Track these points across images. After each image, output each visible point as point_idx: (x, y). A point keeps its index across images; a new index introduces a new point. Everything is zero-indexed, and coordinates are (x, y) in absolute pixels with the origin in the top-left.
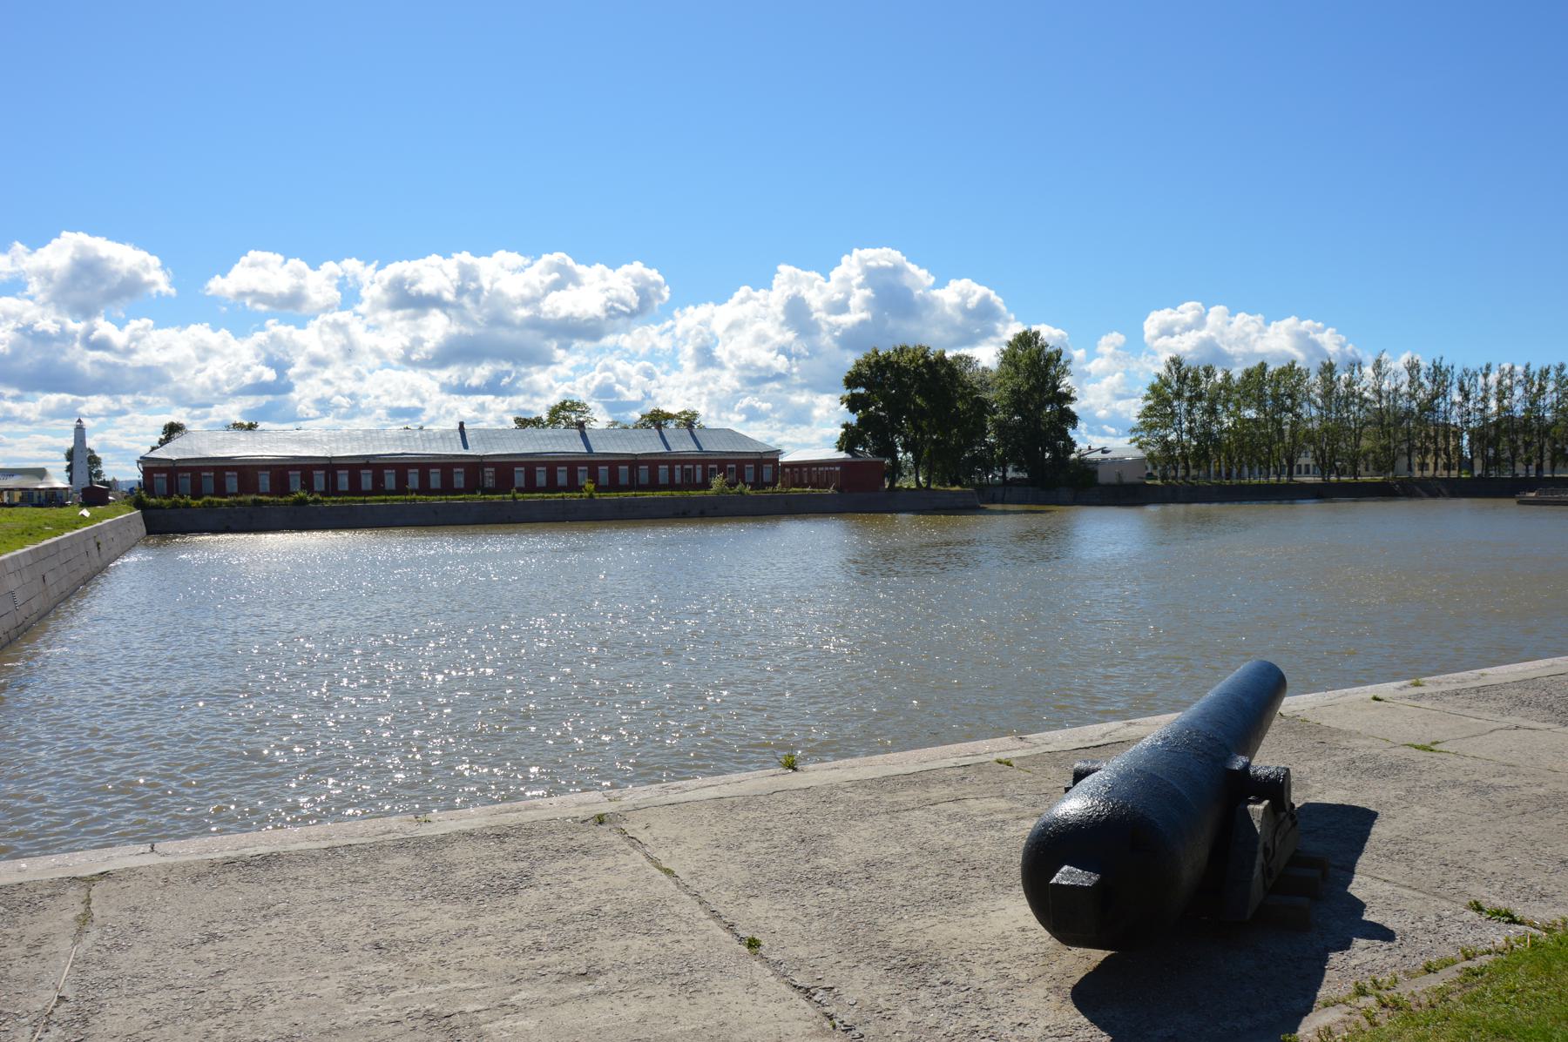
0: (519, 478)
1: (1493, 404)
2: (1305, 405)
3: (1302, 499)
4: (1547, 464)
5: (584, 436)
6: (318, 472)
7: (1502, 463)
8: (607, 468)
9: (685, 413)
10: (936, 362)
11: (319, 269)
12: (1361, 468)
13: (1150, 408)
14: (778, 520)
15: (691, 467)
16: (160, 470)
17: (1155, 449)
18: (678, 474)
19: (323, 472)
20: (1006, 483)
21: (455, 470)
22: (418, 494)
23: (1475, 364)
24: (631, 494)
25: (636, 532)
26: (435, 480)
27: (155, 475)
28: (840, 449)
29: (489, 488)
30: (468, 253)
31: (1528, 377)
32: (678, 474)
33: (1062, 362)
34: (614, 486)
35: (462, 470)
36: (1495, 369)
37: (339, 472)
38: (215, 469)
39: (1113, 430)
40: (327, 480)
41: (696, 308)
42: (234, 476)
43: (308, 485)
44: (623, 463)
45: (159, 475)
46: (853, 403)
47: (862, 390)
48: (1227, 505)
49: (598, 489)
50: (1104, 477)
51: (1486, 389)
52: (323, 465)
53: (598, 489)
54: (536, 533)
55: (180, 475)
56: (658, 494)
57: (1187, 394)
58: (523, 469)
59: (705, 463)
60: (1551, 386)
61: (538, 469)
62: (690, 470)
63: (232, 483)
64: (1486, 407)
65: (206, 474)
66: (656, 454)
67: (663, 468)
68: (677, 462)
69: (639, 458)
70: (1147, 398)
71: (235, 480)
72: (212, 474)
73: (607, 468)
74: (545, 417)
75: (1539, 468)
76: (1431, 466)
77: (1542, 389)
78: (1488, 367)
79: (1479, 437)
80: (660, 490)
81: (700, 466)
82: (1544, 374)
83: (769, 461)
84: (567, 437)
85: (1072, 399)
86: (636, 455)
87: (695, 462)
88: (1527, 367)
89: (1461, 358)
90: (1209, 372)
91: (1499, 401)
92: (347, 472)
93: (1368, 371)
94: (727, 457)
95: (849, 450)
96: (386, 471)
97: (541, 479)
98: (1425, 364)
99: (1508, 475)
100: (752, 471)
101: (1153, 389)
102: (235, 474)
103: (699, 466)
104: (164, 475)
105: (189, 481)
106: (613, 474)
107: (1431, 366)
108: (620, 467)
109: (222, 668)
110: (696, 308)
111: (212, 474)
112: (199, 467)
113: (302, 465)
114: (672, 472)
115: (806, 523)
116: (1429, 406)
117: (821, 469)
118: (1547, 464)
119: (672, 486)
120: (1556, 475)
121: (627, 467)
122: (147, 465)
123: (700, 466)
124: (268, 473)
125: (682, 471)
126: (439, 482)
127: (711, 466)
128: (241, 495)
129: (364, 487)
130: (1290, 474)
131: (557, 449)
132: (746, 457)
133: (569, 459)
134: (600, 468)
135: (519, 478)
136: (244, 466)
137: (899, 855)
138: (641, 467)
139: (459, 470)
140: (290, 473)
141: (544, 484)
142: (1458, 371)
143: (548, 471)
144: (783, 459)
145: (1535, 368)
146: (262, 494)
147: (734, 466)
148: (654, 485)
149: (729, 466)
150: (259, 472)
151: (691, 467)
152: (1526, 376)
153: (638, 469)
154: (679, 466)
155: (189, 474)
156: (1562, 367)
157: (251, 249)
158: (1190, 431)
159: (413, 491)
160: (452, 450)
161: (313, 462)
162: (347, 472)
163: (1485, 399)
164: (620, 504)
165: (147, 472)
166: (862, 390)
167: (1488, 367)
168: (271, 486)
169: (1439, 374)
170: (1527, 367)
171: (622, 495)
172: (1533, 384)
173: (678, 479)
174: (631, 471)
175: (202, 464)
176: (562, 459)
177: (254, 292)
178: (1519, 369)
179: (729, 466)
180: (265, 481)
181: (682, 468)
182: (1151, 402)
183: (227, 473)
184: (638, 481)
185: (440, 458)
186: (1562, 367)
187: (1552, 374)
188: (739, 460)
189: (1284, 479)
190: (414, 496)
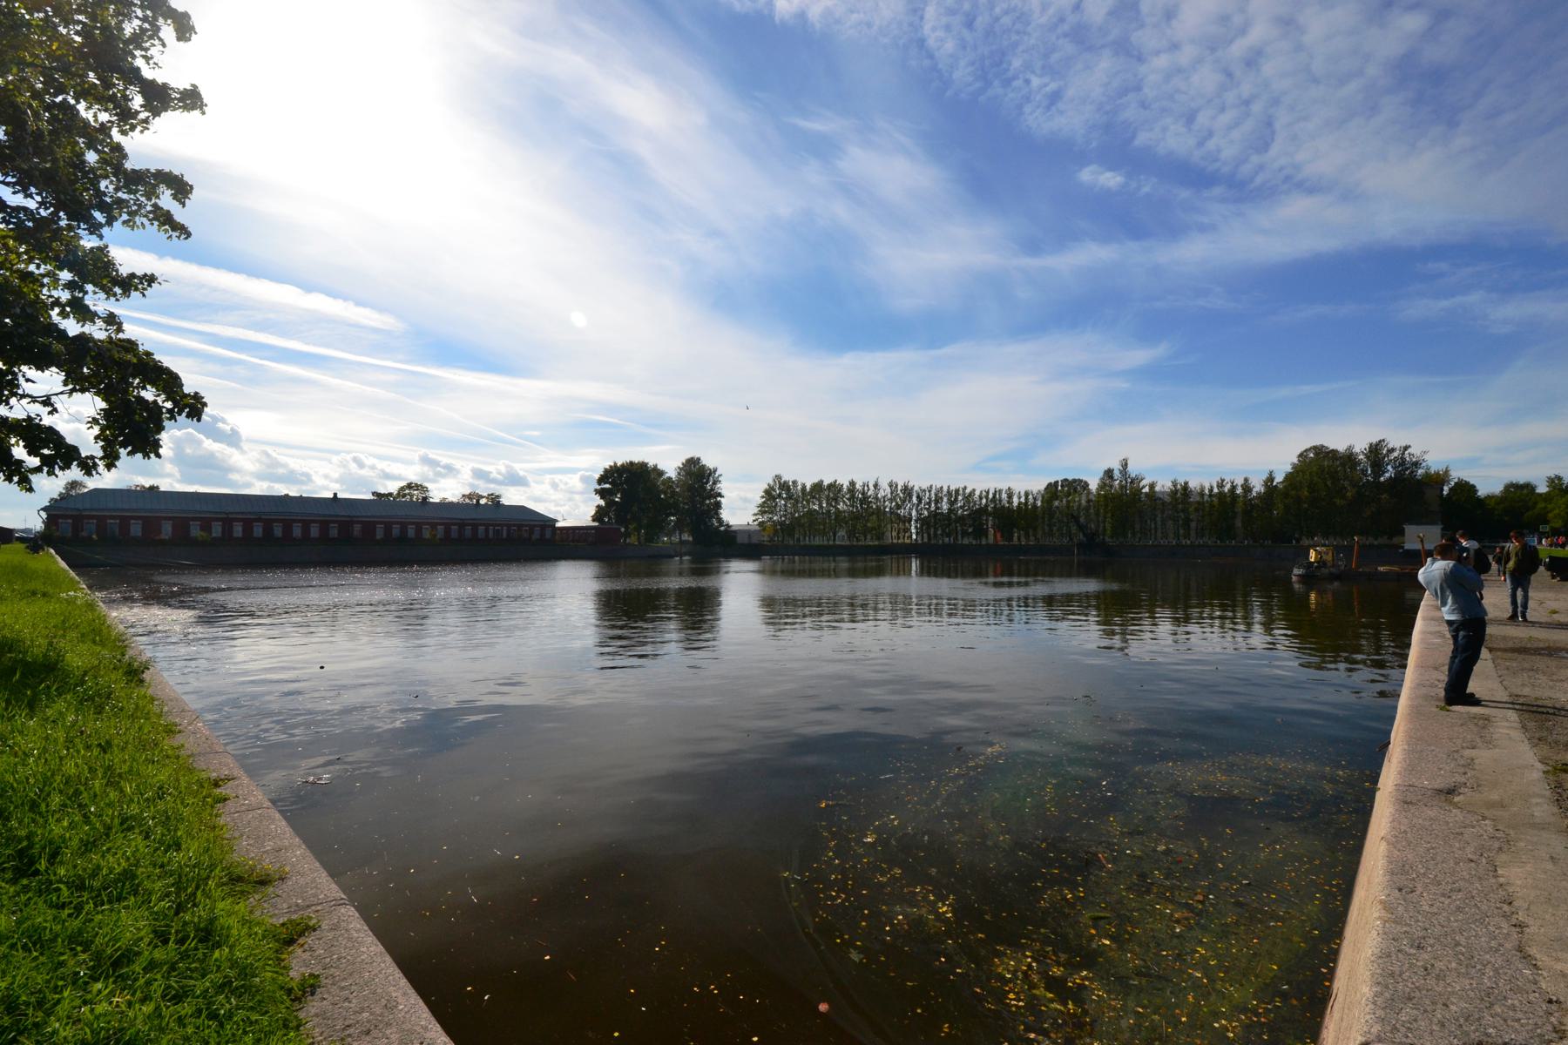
2: (841, 504)
7: (9, 723)
9: (492, 495)
13: (764, 502)
15: (499, 528)
25: (361, 573)
28: (594, 520)
31: (949, 493)
33: (717, 475)
37: (235, 523)
41: (699, 459)
46: (602, 493)
47: (607, 486)
50: (740, 540)
55: (86, 521)
60: (960, 498)
64: (930, 507)
67: (482, 529)
68: (492, 525)
70: (763, 497)
77: (956, 499)
78: (931, 487)
82: (957, 491)
83: (549, 526)
88: (721, 475)
91: (936, 504)
93: (872, 488)
99: (984, 542)
101: (767, 492)
104: (70, 521)
110: (699, 459)
111: (118, 521)
114: (487, 531)
117: (582, 531)
124: (171, 522)
130: (834, 540)
132: (376, 520)
142: (916, 488)
144: (558, 525)
151: (499, 528)
163: (929, 503)
166: (607, 486)
167: (931, 487)
169: (907, 491)
170: (949, 487)
178: (945, 489)
183: (132, 521)
189: (831, 543)
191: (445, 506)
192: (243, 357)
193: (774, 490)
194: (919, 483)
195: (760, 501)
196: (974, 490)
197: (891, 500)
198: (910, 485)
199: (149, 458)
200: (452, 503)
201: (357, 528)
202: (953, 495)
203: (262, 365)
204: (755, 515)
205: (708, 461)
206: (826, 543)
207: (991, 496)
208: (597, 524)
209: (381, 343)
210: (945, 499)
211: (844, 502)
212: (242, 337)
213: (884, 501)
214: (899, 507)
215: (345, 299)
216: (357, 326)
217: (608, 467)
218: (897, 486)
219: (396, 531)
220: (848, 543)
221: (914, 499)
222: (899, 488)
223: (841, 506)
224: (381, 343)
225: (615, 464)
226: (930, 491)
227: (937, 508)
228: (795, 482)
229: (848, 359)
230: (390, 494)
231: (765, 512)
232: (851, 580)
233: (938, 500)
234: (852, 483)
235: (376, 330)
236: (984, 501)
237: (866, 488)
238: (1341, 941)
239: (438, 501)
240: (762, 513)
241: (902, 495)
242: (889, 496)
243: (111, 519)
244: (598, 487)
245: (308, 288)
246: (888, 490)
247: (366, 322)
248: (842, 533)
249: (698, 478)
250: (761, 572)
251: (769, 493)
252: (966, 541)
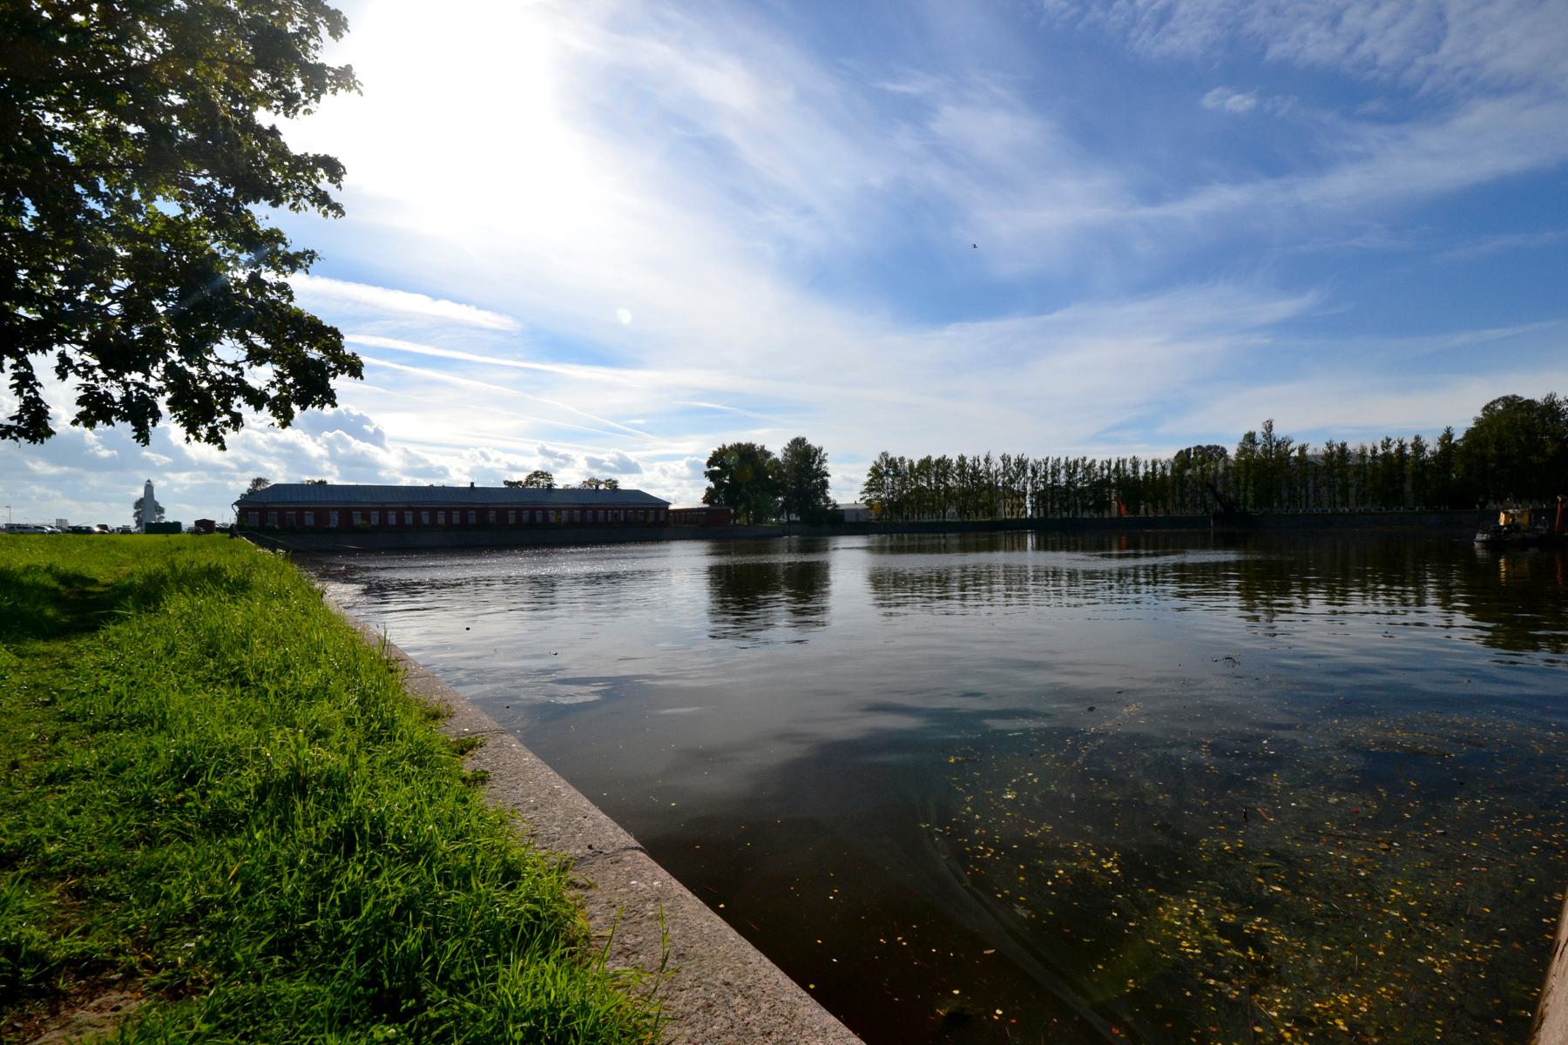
1: (1197, 951)
4: (1079, 510)
12: (980, 513)
18: (610, 515)
20: (790, 522)
28: (704, 502)
31: (1067, 465)
41: (804, 439)
47: (717, 468)
51: (1046, 472)
57: (892, 473)
60: (1079, 470)
67: (601, 513)
70: (870, 475)
75: (1076, 512)
77: (1075, 471)
78: (1047, 459)
79: (1040, 497)
82: (1076, 462)
85: (706, 473)
93: (982, 462)
104: (257, 513)
114: (606, 514)
118: (1079, 510)
130: (944, 517)
137: (770, 1008)
142: (1031, 462)
144: (671, 507)
145: (1071, 459)
160: (343, 476)
163: (1045, 477)
166: (717, 468)
167: (1047, 459)
169: (1021, 464)
178: (1063, 461)
185: (941, 580)
186: (1269, 426)
189: (941, 520)
191: (568, 492)
192: (385, 363)
193: (881, 468)
194: (1034, 455)
195: (867, 479)
196: (1094, 461)
197: (1004, 474)
198: (1025, 458)
199: (1003, 459)
200: (573, 490)
202: (1071, 468)
203: (401, 370)
204: (863, 493)
205: (813, 441)
207: (1113, 467)
208: (707, 506)
209: (502, 344)
210: (1063, 472)
211: (954, 478)
212: (383, 345)
213: (996, 476)
214: (1012, 481)
215: (468, 304)
216: (481, 329)
217: (716, 450)
218: (1009, 460)
219: (526, 516)
220: (958, 520)
221: (1029, 474)
222: (1013, 461)
223: (951, 482)
224: (502, 344)
225: (724, 446)
226: (1046, 464)
227: (1054, 481)
228: (902, 459)
229: (952, 331)
230: (520, 483)
231: (872, 490)
233: (1055, 472)
234: (962, 458)
235: (495, 332)
236: (1106, 472)
237: (977, 463)
239: (561, 487)
240: (869, 491)
241: (1015, 469)
242: (1002, 470)
244: (708, 470)
245: (436, 296)
246: (1001, 464)
247: (487, 324)
248: (952, 510)
249: (804, 458)
250: (869, 549)
251: (875, 471)
252: (1086, 515)
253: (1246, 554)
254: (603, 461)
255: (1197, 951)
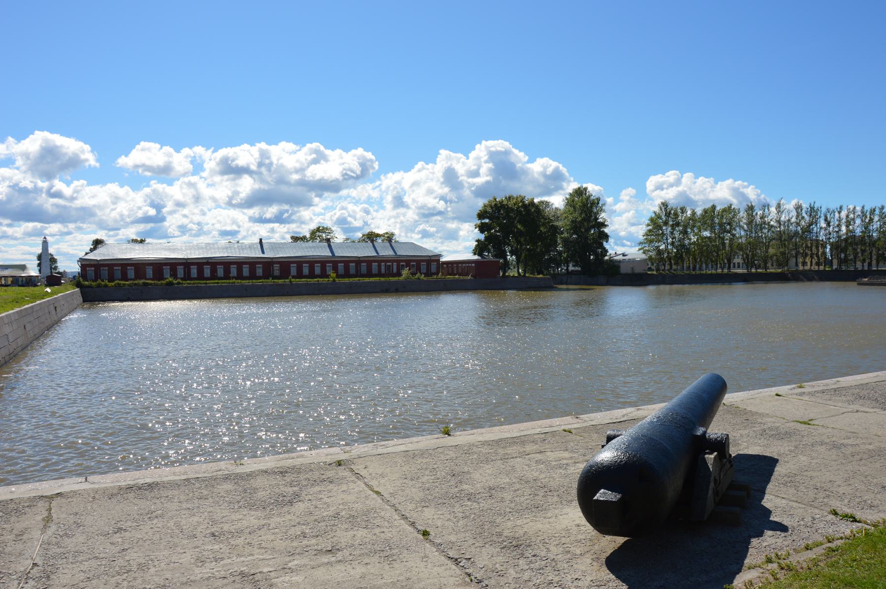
0: (293, 270)
1: (844, 229)
3: (736, 282)
4: (874, 262)
5: (330, 246)
6: (180, 267)
8: (343, 264)
10: (529, 205)
11: (180, 152)
14: (439, 294)
15: (391, 264)
16: (90, 266)
17: (653, 254)
18: (383, 268)
19: (182, 267)
20: (568, 273)
21: (257, 266)
22: (236, 279)
23: (834, 206)
24: (357, 279)
25: (359, 301)
26: (246, 271)
27: (88, 269)
28: (475, 254)
29: (276, 276)
30: (264, 143)
31: (863, 213)
32: (383, 268)
33: (600, 205)
34: (347, 274)
35: (261, 266)
36: (845, 208)
37: (192, 267)
38: (121, 265)
39: (629, 243)
40: (185, 271)
41: (393, 174)
42: (132, 269)
43: (174, 274)
44: (352, 262)
45: (90, 269)
46: (482, 228)
47: (487, 221)
48: (693, 286)
49: (338, 276)
50: (624, 270)
52: (183, 263)
53: (338, 276)
54: (303, 301)
55: (102, 268)
56: (372, 279)
57: (671, 223)
58: (295, 265)
59: (398, 262)
60: (876, 218)
61: (304, 265)
62: (390, 265)
63: (131, 273)
65: (116, 268)
66: (370, 257)
67: (375, 265)
68: (383, 261)
69: (361, 259)
70: (648, 225)
71: (133, 271)
72: (120, 268)
73: (343, 264)
74: (308, 236)
75: (870, 264)
76: (809, 263)
77: (871, 220)
78: (841, 208)
79: (836, 247)
80: (373, 277)
81: (395, 264)
82: (873, 211)
83: (434, 261)
84: (321, 247)
86: (359, 257)
87: (392, 261)
89: (826, 202)
90: (683, 210)
91: (847, 226)
92: (196, 267)
93: (773, 209)
94: (411, 258)
95: (480, 255)
96: (218, 266)
97: (306, 271)
98: (805, 206)
99: (852, 269)
100: (425, 266)
102: (133, 268)
103: (395, 264)
104: (93, 269)
105: (107, 272)
106: (347, 268)
107: (808, 207)
108: (350, 264)
109: (125, 377)
110: (393, 174)
111: (120, 268)
112: (112, 264)
113: (171, 263)
114: (379, 267)
115: (455, 296)
116: (808, 230)
117: (464, 265)
118: (874, 262)
119: (379, 275)
120: (879, 269)
121: (354, 264)
122: (83, 263)
123: (395, 264)
124: (152, 267)
125: (385, 266)
126: (248, 272)
127: (402, 264)
128: (136, 280)
129: (206, 275)
130: (729, 268)
131: (315, 254)
133: (322, 260)
134: (339, 264)
135: (293, 270)
136: (138, 264)
138: (362, 264)
139: (259, 266)
140: (164, 267)
141: (308, 274)
142: (824, 210)
143: (310, 266)
144: (443, 259)
145: (868, 208)
146: (148, 279)
147: (415, 263)
148: (369, 274)
149: (412, 263)
150: (147, 267)
151: (391, 264)
152: (862, 212)
153: (360, 265)
154: (384, 264)
155: (107, 268)
156: (883, 208)
157: (142, 141)
158: (673, 244)
159: (233, 278)
161: (177, 261)
162: (196, 267)
163: (839, 226)
164: (350, 285)
165: (83, 267)
166: (487, 221)
167: (841, 208)
168: (153, 274)
169: (813, 211)
170: (863, 207)
171: (351, 280)
172: (866, 217)
173: (383, 271)
174: (356, 266)
175: (114, 262)
176: (318, 260)
177: (143, 165)
178: (858, 208)
179: (412, 263)
180: (150, 272)
181: (385, 264)
182: (650, 227)
183: (128, 268)
184: (360, 272)
186: (883, 208)
187: (877, 212)
188: (417, 260)
189: (726, 271)
190: (234, 280)
201: (277, 267)
206: (719, 271)
232: (584, 295)
238: (521, 285)
243: (129, 266)
246: (794, 213)
253: (312, 198)
254: (89, 184)
255: (844, 229)
